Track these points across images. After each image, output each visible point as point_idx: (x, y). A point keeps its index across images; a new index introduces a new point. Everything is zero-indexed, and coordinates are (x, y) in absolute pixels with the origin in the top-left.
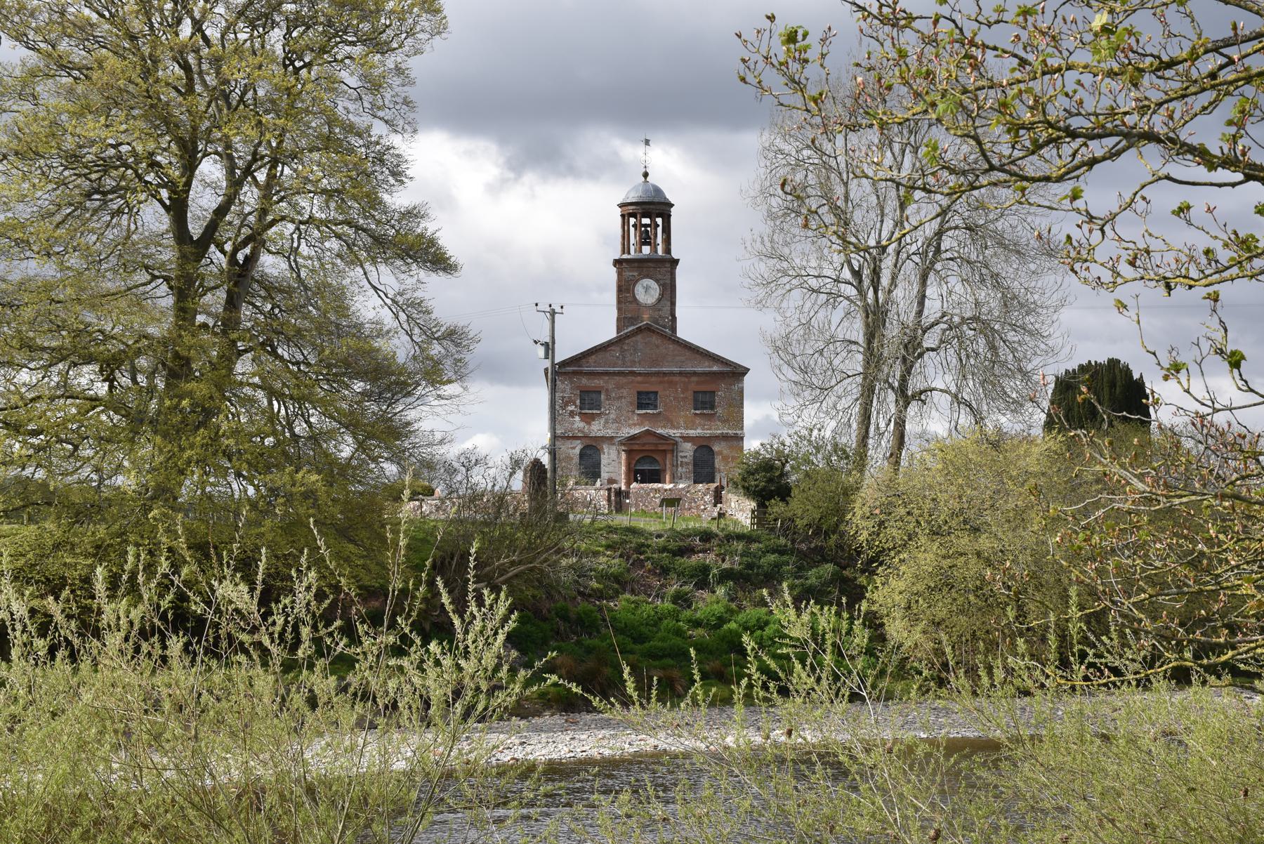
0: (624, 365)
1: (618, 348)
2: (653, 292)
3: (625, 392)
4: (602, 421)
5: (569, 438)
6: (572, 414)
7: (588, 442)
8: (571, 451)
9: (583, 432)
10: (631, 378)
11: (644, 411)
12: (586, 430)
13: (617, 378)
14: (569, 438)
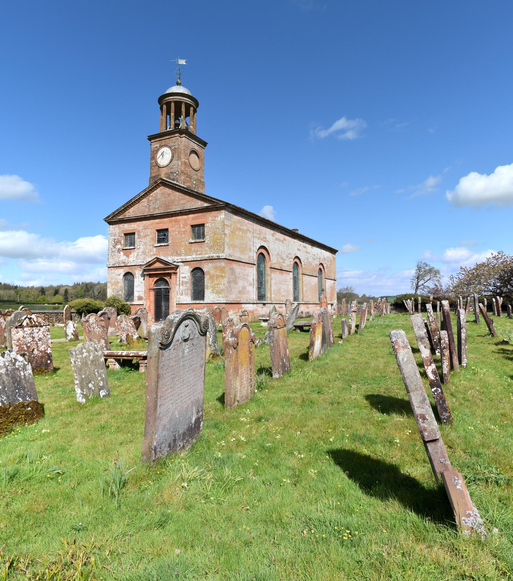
3: (149, 231)
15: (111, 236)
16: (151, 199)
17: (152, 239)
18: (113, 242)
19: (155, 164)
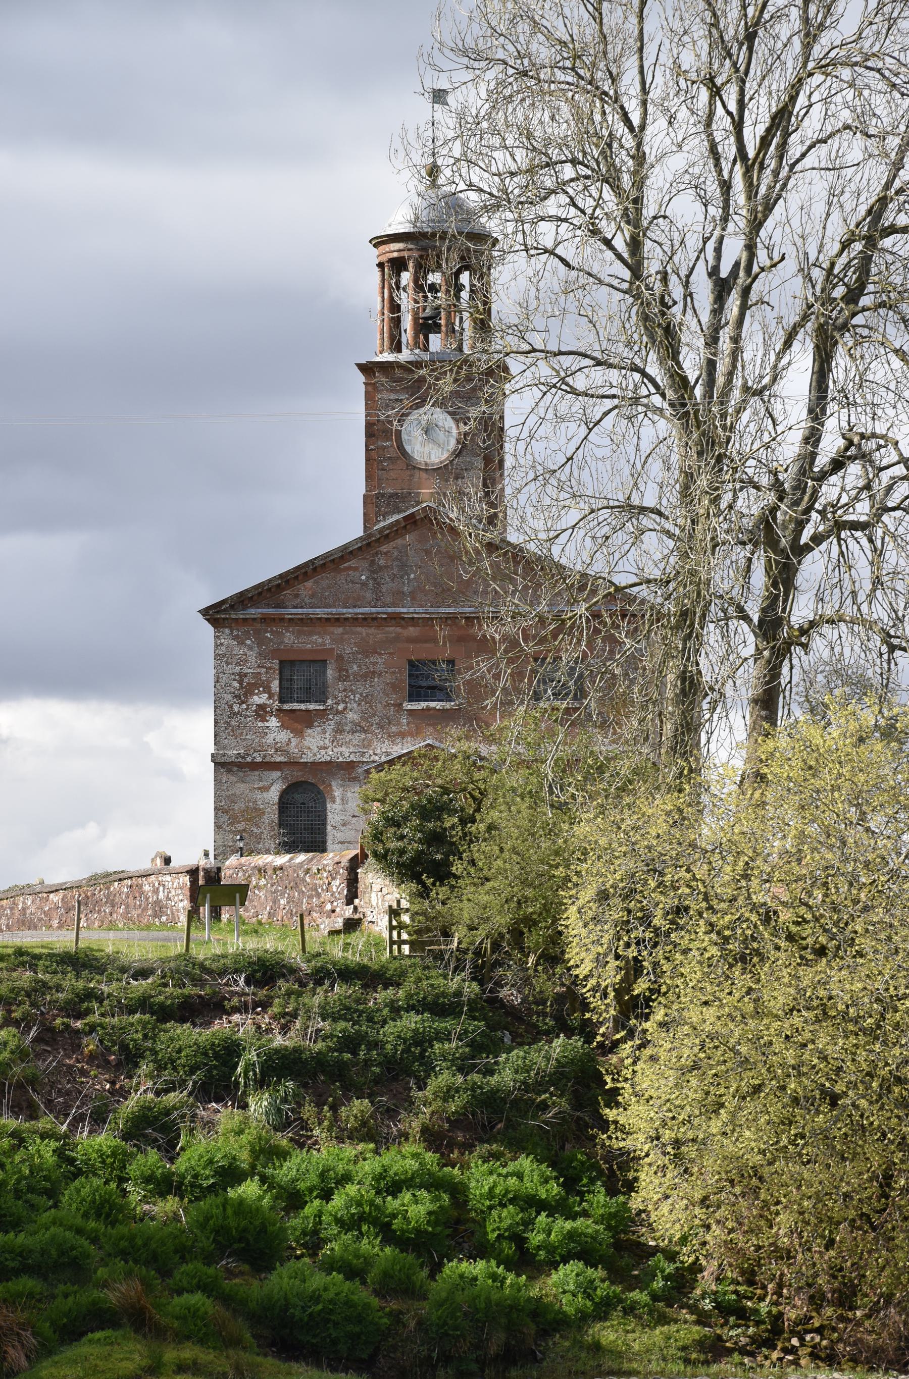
0: (377, 600)
1: (365, 564)
2: (441, 436)
3: (380, 662)
4: (330, 727)
5: (254, 766)
6: (262, 712)
7: (297, 775)
8: (258, 795)
9: (285, 752)
10: (393, 630)
11: (423, 705)
12: (293, 749)
13: (363, 631)
14: (254, 766)
15: (227, 663)
16: (382, 562)
17: (394, 687)
18: (236, 684)
19: (393, 452)
